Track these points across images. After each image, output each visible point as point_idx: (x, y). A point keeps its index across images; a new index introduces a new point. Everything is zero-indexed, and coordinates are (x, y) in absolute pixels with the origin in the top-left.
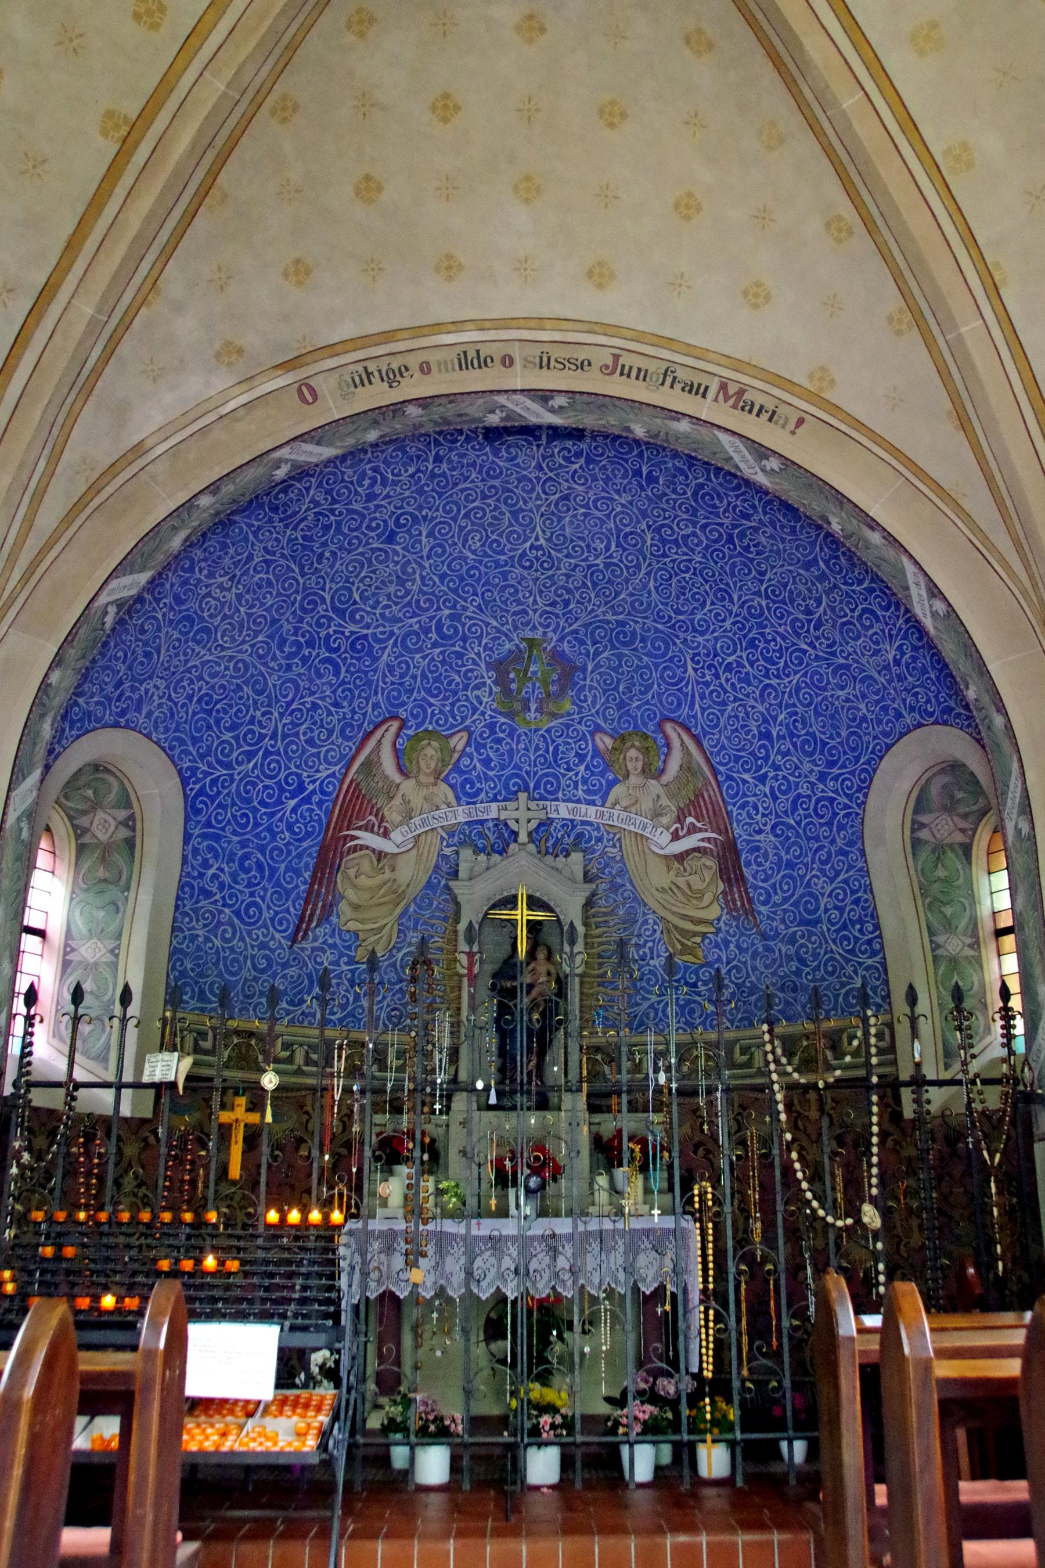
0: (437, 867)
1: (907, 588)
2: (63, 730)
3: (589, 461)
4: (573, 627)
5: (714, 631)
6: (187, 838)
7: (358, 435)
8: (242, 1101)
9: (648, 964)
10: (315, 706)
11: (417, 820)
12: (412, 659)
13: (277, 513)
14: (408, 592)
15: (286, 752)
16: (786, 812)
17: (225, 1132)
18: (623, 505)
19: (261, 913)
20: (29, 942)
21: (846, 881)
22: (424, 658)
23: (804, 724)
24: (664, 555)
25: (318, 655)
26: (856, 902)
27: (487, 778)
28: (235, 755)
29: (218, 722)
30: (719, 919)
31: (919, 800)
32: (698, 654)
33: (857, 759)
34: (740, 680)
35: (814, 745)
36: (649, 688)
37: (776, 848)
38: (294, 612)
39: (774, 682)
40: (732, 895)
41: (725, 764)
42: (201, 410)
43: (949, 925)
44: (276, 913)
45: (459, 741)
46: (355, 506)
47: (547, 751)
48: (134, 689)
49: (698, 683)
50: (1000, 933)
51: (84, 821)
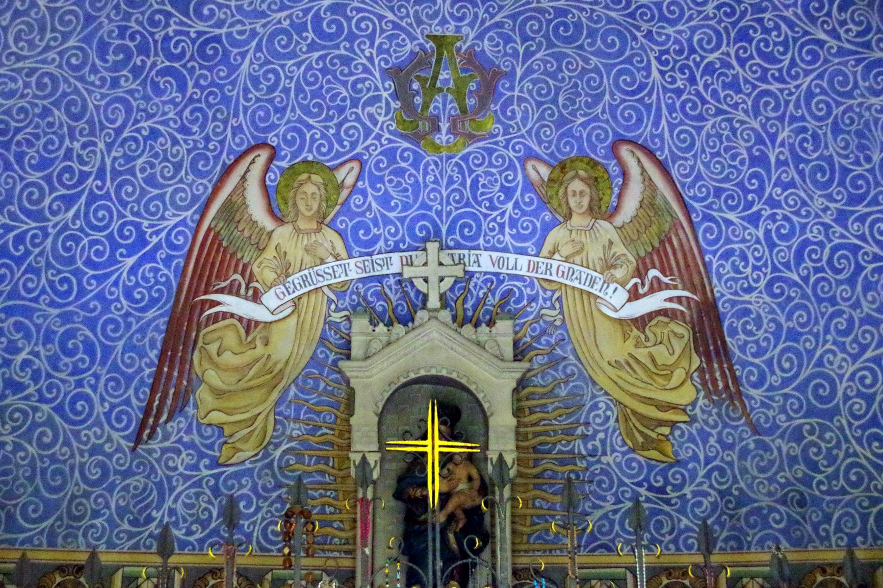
0: (323, 338)
4: (497, 19)
5: (691, 18)
9: (599, 462)
10: (154, 134)
11: (296, 278)
12: (283, 66)
16: (787, 265)
19: (92, 407)
22: (299, 65)
25: (154, 64)
27: (387, 221)
30: (694, 404)
32: (667, 52)
34: (725, 86)
35: (829, 175)
37: (772, 311)
39: (774, 87)
40: (712, 374)
44: (113, 406)
45: (347, 174)
47: (463, 184)
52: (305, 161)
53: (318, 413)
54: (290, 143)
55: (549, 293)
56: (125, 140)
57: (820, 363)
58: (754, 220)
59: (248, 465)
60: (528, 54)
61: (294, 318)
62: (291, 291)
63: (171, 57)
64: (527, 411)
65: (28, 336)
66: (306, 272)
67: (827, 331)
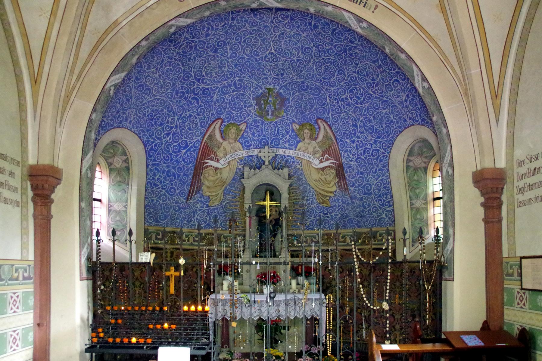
0: (236, 172)
1: (413, 76)
2: (99, 131)
3: (292, 19)
4: (285, 84)
5: (338, 86)
6: (147, 166)
7: (202, 13)
8: (173, 268)
10: (190, 116)
11: (229, 156)
13: (172, 43)
14: (223, 72)
15: (181, 133)
17: (168, 278)
18: (304, 37)
20: (95, 203)
21: (382, 180)
22: (230, 96)
23: (370, 122)
24: (320, 56)
26: (385, 187)
28: (162, 135)
29: (155, 123)
30: (336, 191)
31: (410, 151)
33: (389, 136)
34: (347, 105)
35: (372, 130)
36: (312, 107)
37: (357, 167)
38: (181, 81)
40: (341, 183)
41: (340, 136)
42: (139, 6)
43: (417, 196)
44: (181, 191)
45: (243, 127)
46: (202, 39)
48: (124, 113)
49: (331, 105)
50: (435, 199)
51: (110, 160)
52: (231, 123)
54: (227, 118)
56: (183, 117)
57: (368, 181)
58: (353, 142)
59: (216, 207)
60: (293, 94)
63: (195, 94)
65: (158, 171)
67: (370, 172)
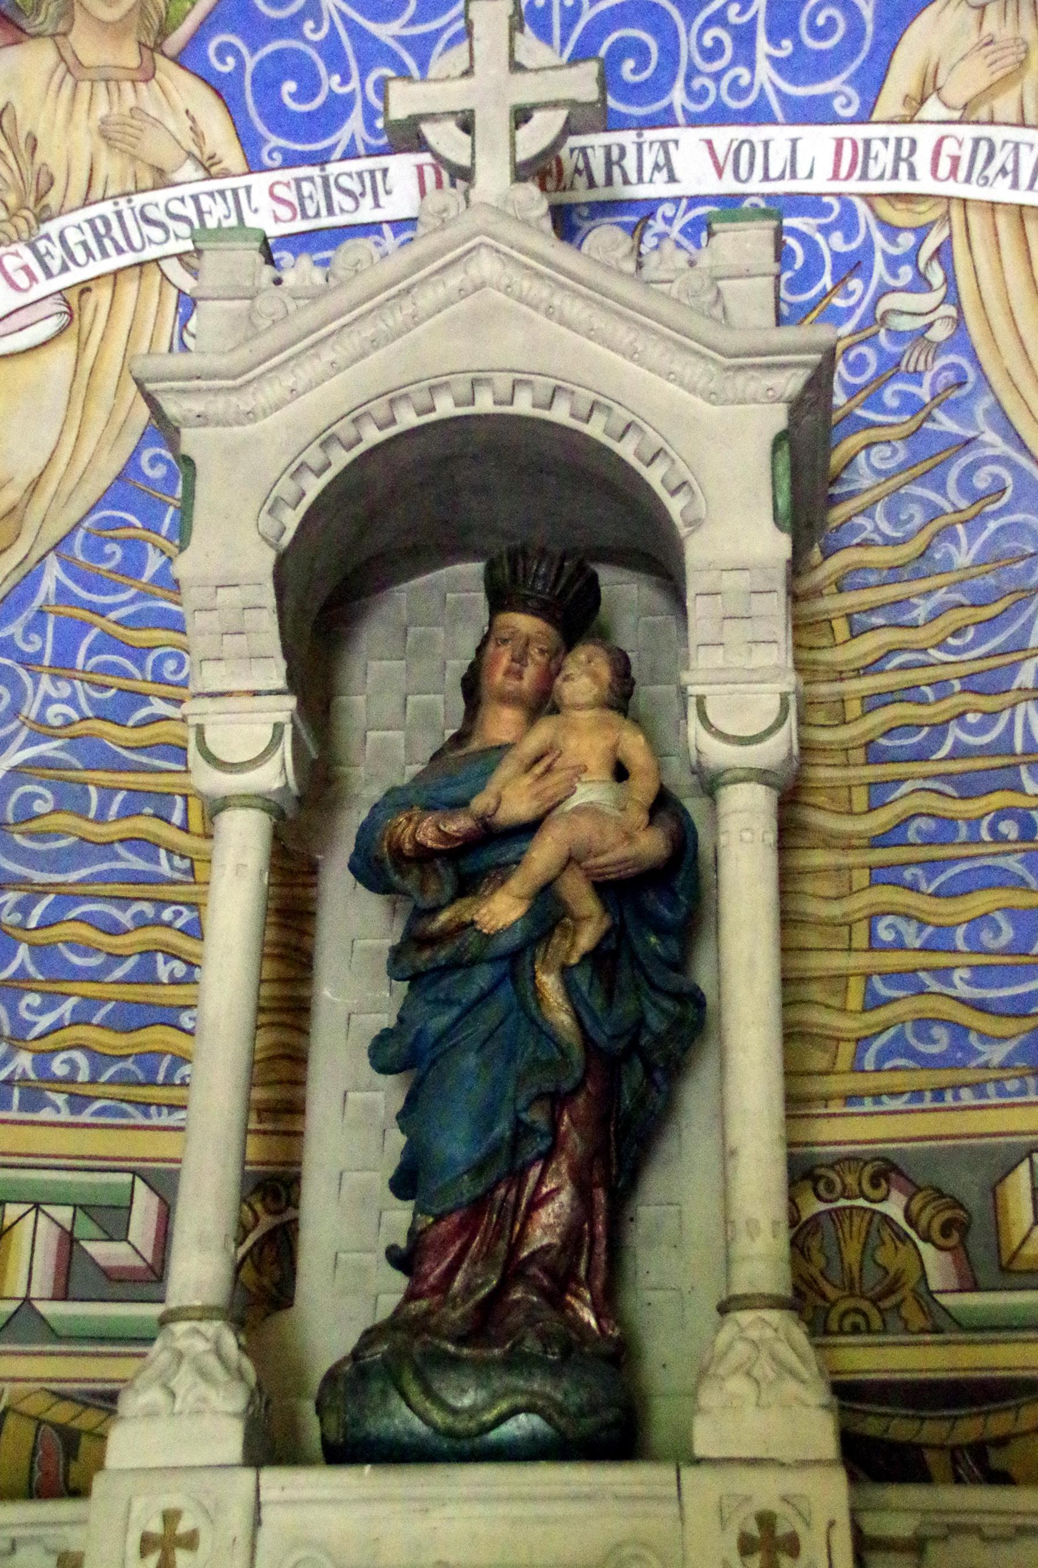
11: (73, 224)
53: (138, 654)
55: (907, 240)
61: (66, 349)
62: (55, 265)
64: (841, 627)
66: (106, 208)
